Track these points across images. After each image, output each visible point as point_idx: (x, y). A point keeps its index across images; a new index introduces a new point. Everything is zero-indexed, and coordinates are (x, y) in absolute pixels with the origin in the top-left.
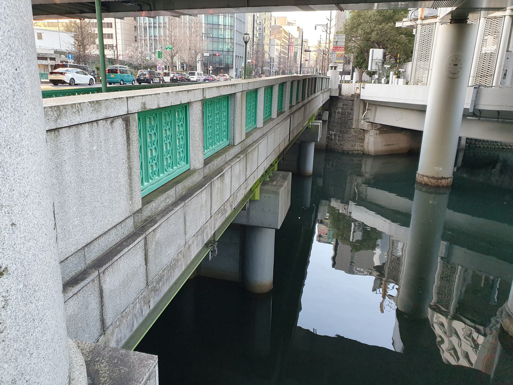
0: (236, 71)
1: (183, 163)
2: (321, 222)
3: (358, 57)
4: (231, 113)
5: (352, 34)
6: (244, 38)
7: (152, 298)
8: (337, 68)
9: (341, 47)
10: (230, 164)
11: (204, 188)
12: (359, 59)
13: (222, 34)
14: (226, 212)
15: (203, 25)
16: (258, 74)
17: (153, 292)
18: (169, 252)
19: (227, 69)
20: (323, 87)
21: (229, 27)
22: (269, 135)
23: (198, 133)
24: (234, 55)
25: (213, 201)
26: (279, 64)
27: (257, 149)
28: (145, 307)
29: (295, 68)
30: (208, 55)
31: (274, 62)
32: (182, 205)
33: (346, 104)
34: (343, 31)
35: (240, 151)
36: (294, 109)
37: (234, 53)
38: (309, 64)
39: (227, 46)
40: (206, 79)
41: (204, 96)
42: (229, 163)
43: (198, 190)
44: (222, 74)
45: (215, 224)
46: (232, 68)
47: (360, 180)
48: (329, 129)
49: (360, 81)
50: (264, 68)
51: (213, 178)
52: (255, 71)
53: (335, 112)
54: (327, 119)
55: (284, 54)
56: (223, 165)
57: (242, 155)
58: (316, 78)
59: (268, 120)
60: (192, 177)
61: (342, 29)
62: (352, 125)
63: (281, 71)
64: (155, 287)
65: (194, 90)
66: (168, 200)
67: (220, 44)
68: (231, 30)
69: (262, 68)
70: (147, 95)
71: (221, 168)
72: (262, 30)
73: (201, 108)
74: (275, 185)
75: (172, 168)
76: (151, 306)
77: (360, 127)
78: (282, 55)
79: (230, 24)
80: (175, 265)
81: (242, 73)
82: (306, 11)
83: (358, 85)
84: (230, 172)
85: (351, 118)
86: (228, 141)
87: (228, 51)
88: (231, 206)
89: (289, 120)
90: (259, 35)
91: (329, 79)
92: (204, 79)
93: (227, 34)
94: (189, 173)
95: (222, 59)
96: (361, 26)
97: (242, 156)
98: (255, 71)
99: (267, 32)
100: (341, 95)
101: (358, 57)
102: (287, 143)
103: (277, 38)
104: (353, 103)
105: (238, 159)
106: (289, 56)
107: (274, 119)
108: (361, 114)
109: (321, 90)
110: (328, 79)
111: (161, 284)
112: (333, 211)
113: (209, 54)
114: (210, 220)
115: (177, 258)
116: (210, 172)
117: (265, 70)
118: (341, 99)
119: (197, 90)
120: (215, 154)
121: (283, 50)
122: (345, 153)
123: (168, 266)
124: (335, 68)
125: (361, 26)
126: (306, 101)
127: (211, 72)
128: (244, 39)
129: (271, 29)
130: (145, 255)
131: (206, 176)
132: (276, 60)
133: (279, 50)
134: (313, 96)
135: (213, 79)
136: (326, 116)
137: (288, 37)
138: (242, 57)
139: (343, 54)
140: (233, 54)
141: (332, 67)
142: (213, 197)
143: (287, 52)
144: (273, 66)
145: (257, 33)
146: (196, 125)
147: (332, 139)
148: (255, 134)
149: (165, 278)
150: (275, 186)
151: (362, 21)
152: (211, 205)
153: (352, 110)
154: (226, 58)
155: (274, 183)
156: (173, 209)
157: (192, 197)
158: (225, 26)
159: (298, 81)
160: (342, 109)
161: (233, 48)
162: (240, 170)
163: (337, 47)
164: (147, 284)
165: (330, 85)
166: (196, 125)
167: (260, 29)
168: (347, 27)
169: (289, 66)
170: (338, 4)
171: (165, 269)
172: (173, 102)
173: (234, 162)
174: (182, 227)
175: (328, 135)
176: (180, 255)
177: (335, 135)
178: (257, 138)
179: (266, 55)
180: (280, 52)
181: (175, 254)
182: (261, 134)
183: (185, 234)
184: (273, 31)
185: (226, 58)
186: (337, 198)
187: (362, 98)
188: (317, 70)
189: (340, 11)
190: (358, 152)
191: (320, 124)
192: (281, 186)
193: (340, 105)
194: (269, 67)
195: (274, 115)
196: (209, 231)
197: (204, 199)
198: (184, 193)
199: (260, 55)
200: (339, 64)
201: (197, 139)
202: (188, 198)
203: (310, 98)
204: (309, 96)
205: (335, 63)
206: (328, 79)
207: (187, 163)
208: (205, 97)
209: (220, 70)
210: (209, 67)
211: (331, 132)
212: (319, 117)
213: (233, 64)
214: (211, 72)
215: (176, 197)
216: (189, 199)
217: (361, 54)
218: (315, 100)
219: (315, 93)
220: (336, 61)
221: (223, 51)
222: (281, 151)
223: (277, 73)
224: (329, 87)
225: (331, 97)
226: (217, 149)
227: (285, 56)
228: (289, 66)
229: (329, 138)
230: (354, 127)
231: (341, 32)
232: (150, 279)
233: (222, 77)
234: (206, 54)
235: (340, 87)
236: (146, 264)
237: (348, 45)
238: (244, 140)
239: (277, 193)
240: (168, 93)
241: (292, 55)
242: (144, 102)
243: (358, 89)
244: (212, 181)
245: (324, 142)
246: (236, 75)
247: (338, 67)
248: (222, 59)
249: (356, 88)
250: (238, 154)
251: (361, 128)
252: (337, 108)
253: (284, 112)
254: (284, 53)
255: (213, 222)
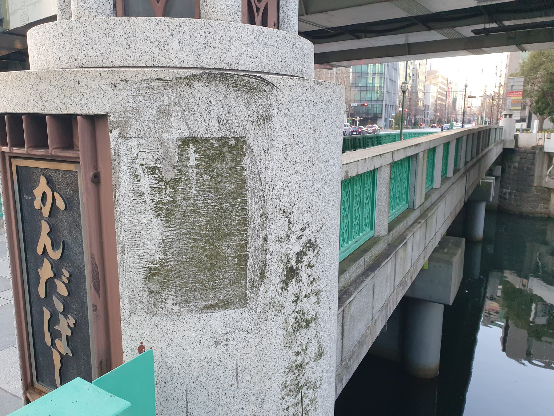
0: (385, 121)
1: (367, 229)
2: (492, 299)
3: (538, 101)
4: (412, 174)
5: (531, 76)
6: (401, 87)
7: (345, 376)
8: (512, 116)
9: (517, 92)
10: (412, 231)
11: (390, 257)
12: (540, 104)
13: (371, 82)
14: (407, 285)
15: (351, 74)
16: (410, 123)
17: (346, 370)
18: (360, 327)
19: (375, 119)
20: (497, 139)
21: (379, 74)
22: (447, 196)
23: (385, 198)
24: (384, 104)
25: (397, 272)
26: (435, 112)
27: (436, 213)
28: (339, 385)
29: (454, 116)
30: (355, 105)
31: (428, 110)
32: (372, 276)
33: (524, 157)
34: (519, 73)
35: (419, 215)
36: (469, 165)
37: (384, 102)
38: (471, 111)
39: (376, 95)
40: (354, 131)
41: (393, 159)
42: (410, 229)
43: (385, 260)
44: (371, 125)
45: (397, 298)
46: (381, 118)
47: (543, 249)
48: (502, 187)
49: (541, 129)
50: (418, 117)
51: (398, 246)
52: (407, 120)
53: (510, 167)
54: (500, 175)
55: (441, 101)
56: (405, 232)
57: (422, 219)
58: (490, 129)
59: (445, 179)
60: (378, 245)
61: (518, 71)
62: (533, 182)
63: (437, 120)
64: (347, 364)
65: (385, 153)
66: (358, 269)
67: (369, 93)
68: (381, 78)
69: (415, 116)
70: (350, 163)
71: (402, 234)
72: (415, 76)
73: (389, 172)
74: (446, 253)
75: (359, 235)
76: (343, 384)
77: (544, 185)
78: (439, 102)
79: (380, 71)
80: (364, 341)
81: (392, 123)
82: (477, 55)
83: (540, 135)
84: (412, 240)
85: (531, 174)
86: (407, 205)
87: (377, 100)
88: (411, 277)
89: (465, 178)
90: (412, 82)
91: (502, 128)
92: (352, 131)
93: (376, 82)
94: (373, 241)
95: (370, 109)
96: (544, 66)
97: (423, 221)
98: (407, 120)
99: (422, 77)
100: (518, 147)
101: (538, 101)
102: (463, 204)
103: (433, 84)
104: (534, 156)
105: (419, 225)
106: (447, 103)
107: (450, 178)
108: (545, 170)
109: (495, 142)
110: (501, 129)
111: (352, 361)
112: (505, 283)
113: (356, 104)
114: (393, 294)
115: (365, 334)
116: (393, 239)
117: (418, 119)
118: (518, 152)
119: (388, 154)
120: (396, 219)
121: (439, 96)
122: (522, 216)
123: (358, 342)
124: (510, 116)
125: (544, 66)
126: (480, 155)
127: (358, 123)
128: (401, 89)
129: (426, 74)
130: (342, 329)
131: (389, 244)
132: (432, 108)
133: (435, 97)
134: (487, 150)
135: (361, 130)
136: (498, 170)
137: (446, 82)
138: (393, 106)
139: (520, 99)
140: (383, 103)
141: (506, 115)
142: (397, 268)
143: (445, 98)
144: (428, 114)
145: (410, 80)
146: (383, 189)
147: (505, 199)
148: (433, 195)
149: (356, 354)
150: (447, 253)
151: (545, 60)
152: (395, 277)
153: (533, 164)
154: (374, 107)
155: (446, 250)
156: (364, 281)
157: (380, 267)
158: (374, 74)
159: (473, 134)
160: (519, 163)
161: (383, 97)
162: (420, 237)
163: (513, 92)
164: (342, 360)
165: (503, 135)
166: (383, 189)
167: (413, 75)
168: (524, 68)
169: (446, 113)
170: (520, 44)
171: (355, 345)
172: (368, 168)
173: (416, 228)
174: (371, 300)
175: (501, 194)
176: (368, 330)
177: (510, 194)
178: (435, 200)
179: (419, 102)
180: (437, 99)
181: (364, 330)
182: (438, 196)
183: (373, 308)
184: (428, 77)
185: (374, 107)
186: (511, 268)
187: (546, 150)
188: (482, 118)
189: (521, 52)
190: (541, 215)
191: (492, 181)
192: (455, 254)
193: (518, 158)
194: (423, 115)
195: (450, 173)
196: (392, 306)
197: (389, 270)
198: (371, 263)
199: (413, 103)
200: (515, 112)
201: (384, 204)
202: (376, 269)
203: (484, 152)
204: (483, 150)
205: (510, 110)
206: (501, 129)
207: (371, 229)
208: (394, 160)
209: (368, 121)
210: (356, 118)
211: (505, 190)
212: (490, 173)
213: (382, 114)
214: (358, 123)
215: (365, 266)
216: (378, 269)
217: (543, 98)
218: (489, 153)
219: (488, 145)
220: (512, 108)
221: (371, 100)
222: (457, 214)
223: (432, 122)
224: (503, 138)
225: (505, 149)
226: (398, 214)
227: (442, 102)
228: (446, 113)
229: (501, 197)
230: (535, 184)
231: (517, 74)
232: (344, 355)
233: (371, 128)
234: (354, 105)
235: (516, 137)
236: (342, 339)
237: (526, 88)
238: (423, 203)
239: (449, 263)
240: (366, 159)
241: (451, 100)
242: (347, 170)
243: (540, 140)
244: (397, 250)
245: (497, 202)
246: (385, 125)
247: (514, 115)
248: (370, 109)
249: (538, 139)
250: (418, 219)
251: (545, 186)
252: (513, 163)
253: (460, 169)
254: (441, 100)
255: (395, 296)
